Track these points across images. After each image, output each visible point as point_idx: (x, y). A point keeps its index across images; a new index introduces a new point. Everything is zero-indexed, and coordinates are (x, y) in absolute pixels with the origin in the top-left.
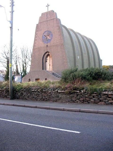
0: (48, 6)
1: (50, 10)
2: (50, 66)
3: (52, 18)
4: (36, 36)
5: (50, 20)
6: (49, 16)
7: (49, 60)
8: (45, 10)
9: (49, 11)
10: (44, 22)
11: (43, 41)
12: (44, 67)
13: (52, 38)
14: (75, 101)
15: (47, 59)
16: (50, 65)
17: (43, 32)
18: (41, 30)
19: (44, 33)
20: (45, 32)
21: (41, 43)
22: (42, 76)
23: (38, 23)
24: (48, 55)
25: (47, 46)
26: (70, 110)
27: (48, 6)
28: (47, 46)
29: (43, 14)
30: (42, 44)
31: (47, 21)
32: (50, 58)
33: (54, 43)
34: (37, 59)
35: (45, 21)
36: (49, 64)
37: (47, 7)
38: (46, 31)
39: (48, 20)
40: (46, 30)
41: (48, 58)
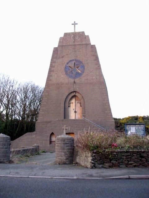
0: (75, 24)
1: (77, 30)
2: (77, 114)
3: (84, 43)
4: (53, 64)
5: (80, 45)
6: (77, 38)
7: (74, 104)
8: (71, 30)
9: (77, 31)
10: (69, 45)
11: (66, 74)
12: (66, 115)
13: (83, 72)
14: (113, 158)
15: (72, 102)
16: (75, 112)
17: (66, 60)
18: (63, 57)
19: (69, 62)
20: (71, 61)
21: (62, 76)
22: (56, 129)
23: (57, 46)
24: (75, 96)
25: (74, 82)
26: (145, 178)
27: (75, 24)
28: (74, 82)
29: (66, 34)
30: (63, 78)
31: (75, 45)
32: (76, 102)
33: (87, 80)
34: (53, 101)
35: (71, 45)
36: (74, 110)
37: (74, 25)
38: (73, 60)
39: (77, 45)
40: (73, 58)
41: (73, 101)
